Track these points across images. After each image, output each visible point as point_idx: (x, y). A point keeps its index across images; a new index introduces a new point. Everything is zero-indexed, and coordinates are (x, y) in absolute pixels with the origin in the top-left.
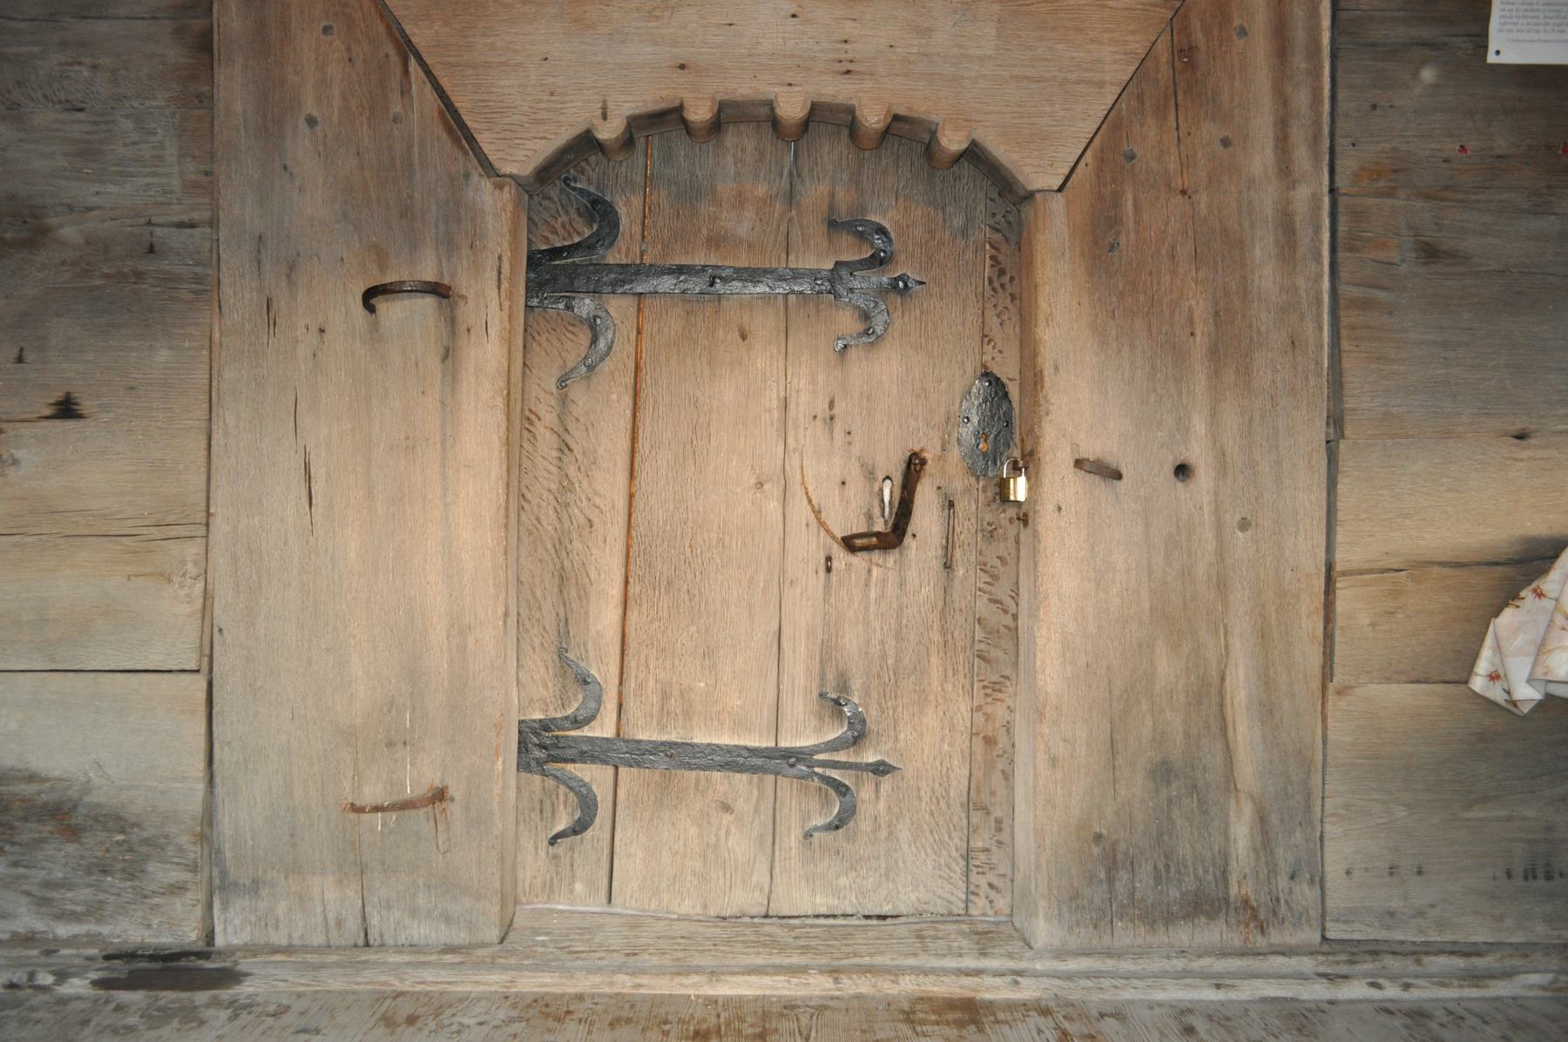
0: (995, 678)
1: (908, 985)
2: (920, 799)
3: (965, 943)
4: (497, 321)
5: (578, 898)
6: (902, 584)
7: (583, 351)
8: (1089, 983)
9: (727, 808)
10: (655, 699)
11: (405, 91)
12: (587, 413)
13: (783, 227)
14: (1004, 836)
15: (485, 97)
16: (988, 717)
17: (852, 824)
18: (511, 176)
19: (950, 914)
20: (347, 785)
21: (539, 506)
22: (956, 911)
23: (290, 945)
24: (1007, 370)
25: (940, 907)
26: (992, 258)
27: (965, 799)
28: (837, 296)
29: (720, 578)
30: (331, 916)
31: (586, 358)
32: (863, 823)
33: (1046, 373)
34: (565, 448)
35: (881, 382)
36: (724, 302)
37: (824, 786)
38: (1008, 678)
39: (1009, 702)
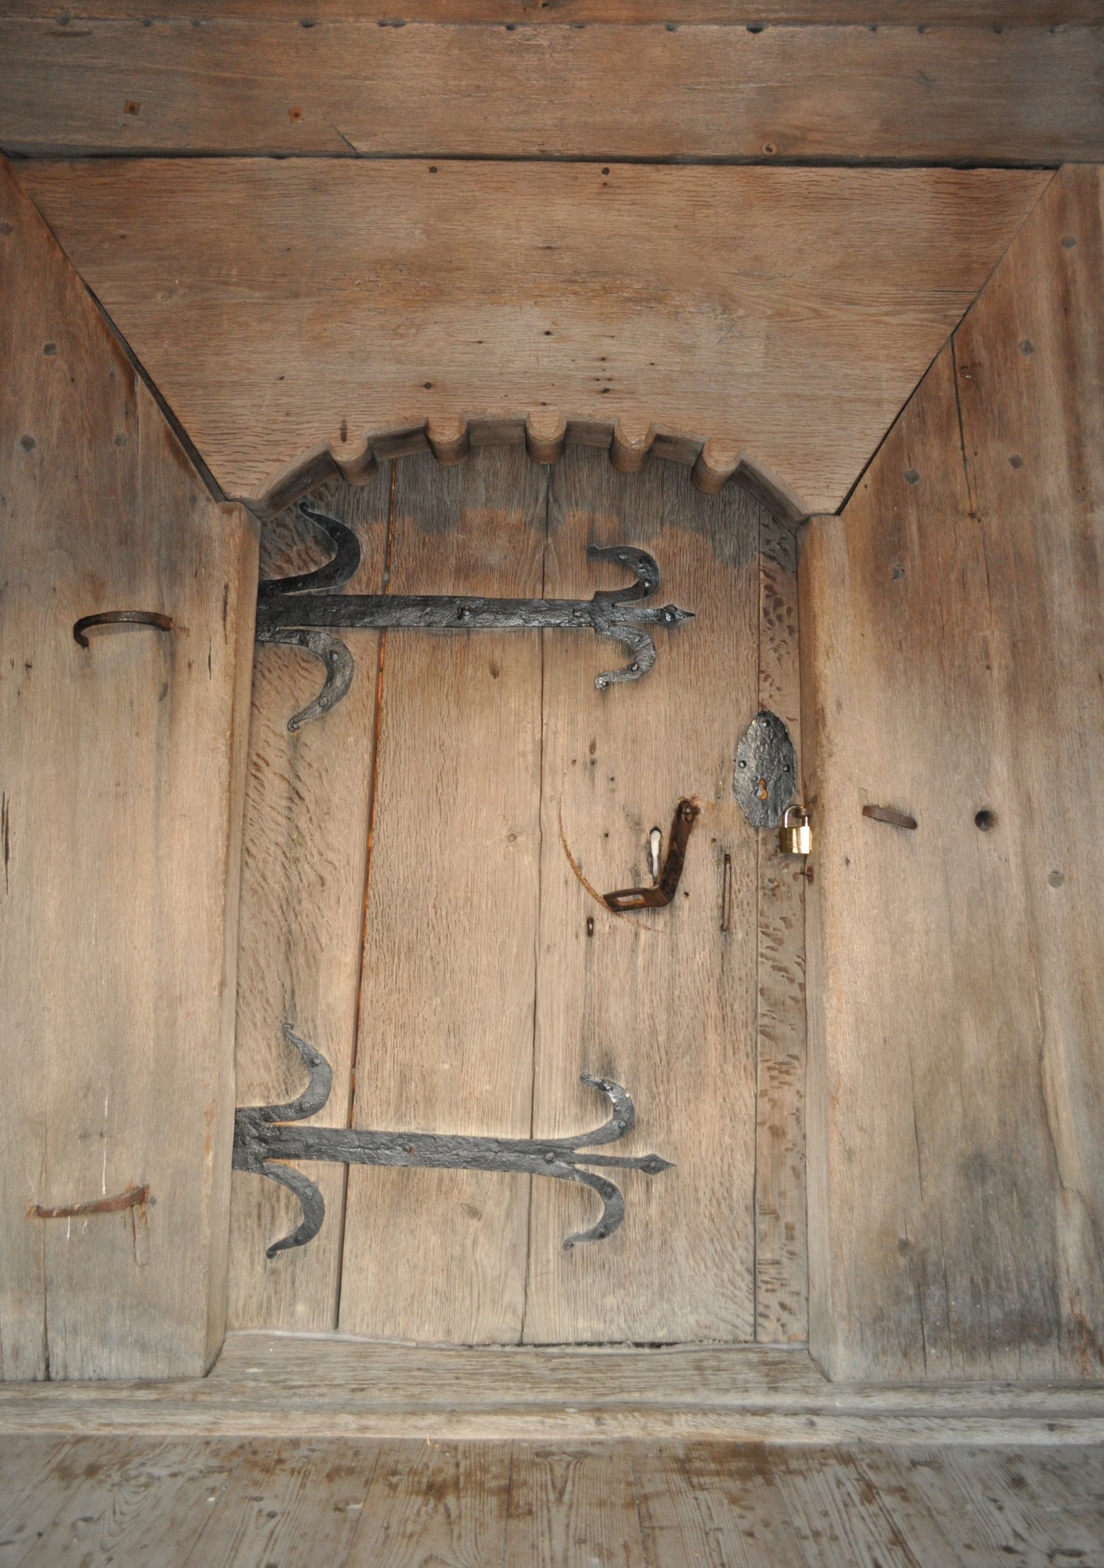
0: (781, 1058)
1: (683, 1429)
2: (698, 1201)
3: (751, 1375)
5: (301, 1323)
6: (673, 949)
7: (318, 689)
8: (898, 1424)
9: (474, 1213)
10: (393, 1084)
11: (130, 412)
12: (321, 758)
13: (539, 556)
14: (797, 1246)
16: (774, 1103)
17: (619, 1231)
18: (241, 500)
19: (736, 1341)
21: (265, 861)
22: (742, 1337)
24: (787, 709)
26: (767, 587)
27: (750, 1201)
28: (598, 629)
29: (467, 942)
32: (633, 1231)
33: (827, 711)
35: (647, 723)
36: (473, 637)
37: (587, 1186)
38: (796, 1058)
39: (799, 1086)
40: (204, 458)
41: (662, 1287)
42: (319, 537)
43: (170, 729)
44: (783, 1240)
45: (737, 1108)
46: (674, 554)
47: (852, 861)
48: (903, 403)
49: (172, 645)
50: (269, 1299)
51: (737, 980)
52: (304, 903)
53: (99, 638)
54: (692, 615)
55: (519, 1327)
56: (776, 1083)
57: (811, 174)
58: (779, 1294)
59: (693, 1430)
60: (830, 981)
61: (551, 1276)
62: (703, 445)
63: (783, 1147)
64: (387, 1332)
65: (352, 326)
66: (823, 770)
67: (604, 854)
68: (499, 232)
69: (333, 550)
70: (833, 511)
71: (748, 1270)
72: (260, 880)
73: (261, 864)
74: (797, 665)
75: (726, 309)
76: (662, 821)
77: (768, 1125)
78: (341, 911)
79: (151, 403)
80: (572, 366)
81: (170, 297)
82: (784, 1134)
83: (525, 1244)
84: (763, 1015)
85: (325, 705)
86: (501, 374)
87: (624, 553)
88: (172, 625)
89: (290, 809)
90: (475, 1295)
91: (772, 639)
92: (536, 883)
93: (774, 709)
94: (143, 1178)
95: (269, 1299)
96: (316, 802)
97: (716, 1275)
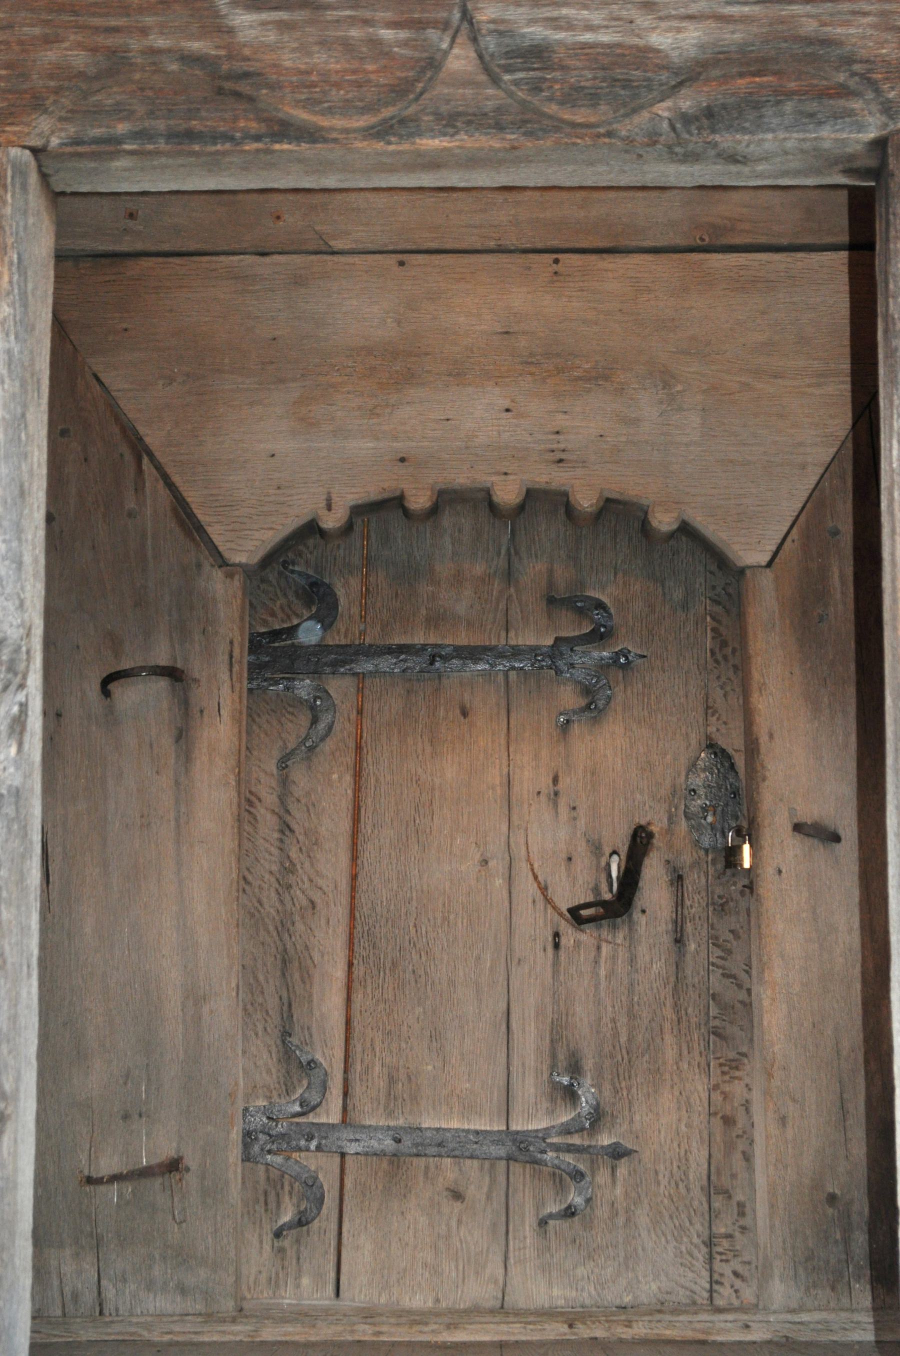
0: (732, 1055)
2: (658, 1183)
4: (229, 702)
5: (308, 1290)
6: (632, 960)
7: (303, 733)
9: (457, 1195)
10: (382, 1084)
11: (139, 488)
12: (308, 794)
13: (502, 606)
14: (747, 1221)
15: (214, 492)
16: (725, 1096)
18: (240, 565)
20: (84, 1157)
23: (852, 247)
24: (733, 742)
25: (682, 1296)
26: (713, 630)
27: (705, 1182)
28: (558, 672)
29: (445, 957)
30: (67, 1290)
31: (306, 739)
32: (602, 1212)
33: (761, 741)
34: (286, 828)
35: (605, 756)
36: (445, 681)
39: (747, 1080)
40: (205, 527)
41: (626, 1258)
42: (300, 592)
43: (186, 767)
44: (735, 1216)
45: (692, 1100)
46: (627, 601)
47: (784, 871)
48: (826, 465)
49: (185, 694)
50: (277, 1274)
51: (691, 988)
52: (297, 924)
53: (120, 689)
54: (645, 657)
55: (500, 1296)
56: (727, 1078)
57: (740, 259)
58: (732, 1263)
59: (649, 1331)
60: (766, 975)
61: (527, 1251)
62: (648, 507)
63: (734, 1135)
64: (382, 1301)
65: (334, 408)
66: (758, 793)
67: (568, 876)
68: (462, 319)
69: (314, 604)
70: (764, 564)
71: (704, 1243)
72: (256, 904)
73: (257, 890)
74: (741, 701)
75: (666, 385)
76: (620, 845)
77: (720, 1115)
78: (330, 931)
79: (157, 480)
80: (529, 439)
81: (170, 384)
82: (735, 1122)
83: (504, 1224)
84: (715, 1018)
85: (309, 749)
86: (467, 448)
87: (581, 601)
88: (184, 677)
89: (281, 841)
90: (461, 1268)
91: (718, 678)
92: (507, 903)
93: (722, 742)
94: (178, 1150)
95: (277, 1274)
96: (305, 834)
97: (675, 1247)
